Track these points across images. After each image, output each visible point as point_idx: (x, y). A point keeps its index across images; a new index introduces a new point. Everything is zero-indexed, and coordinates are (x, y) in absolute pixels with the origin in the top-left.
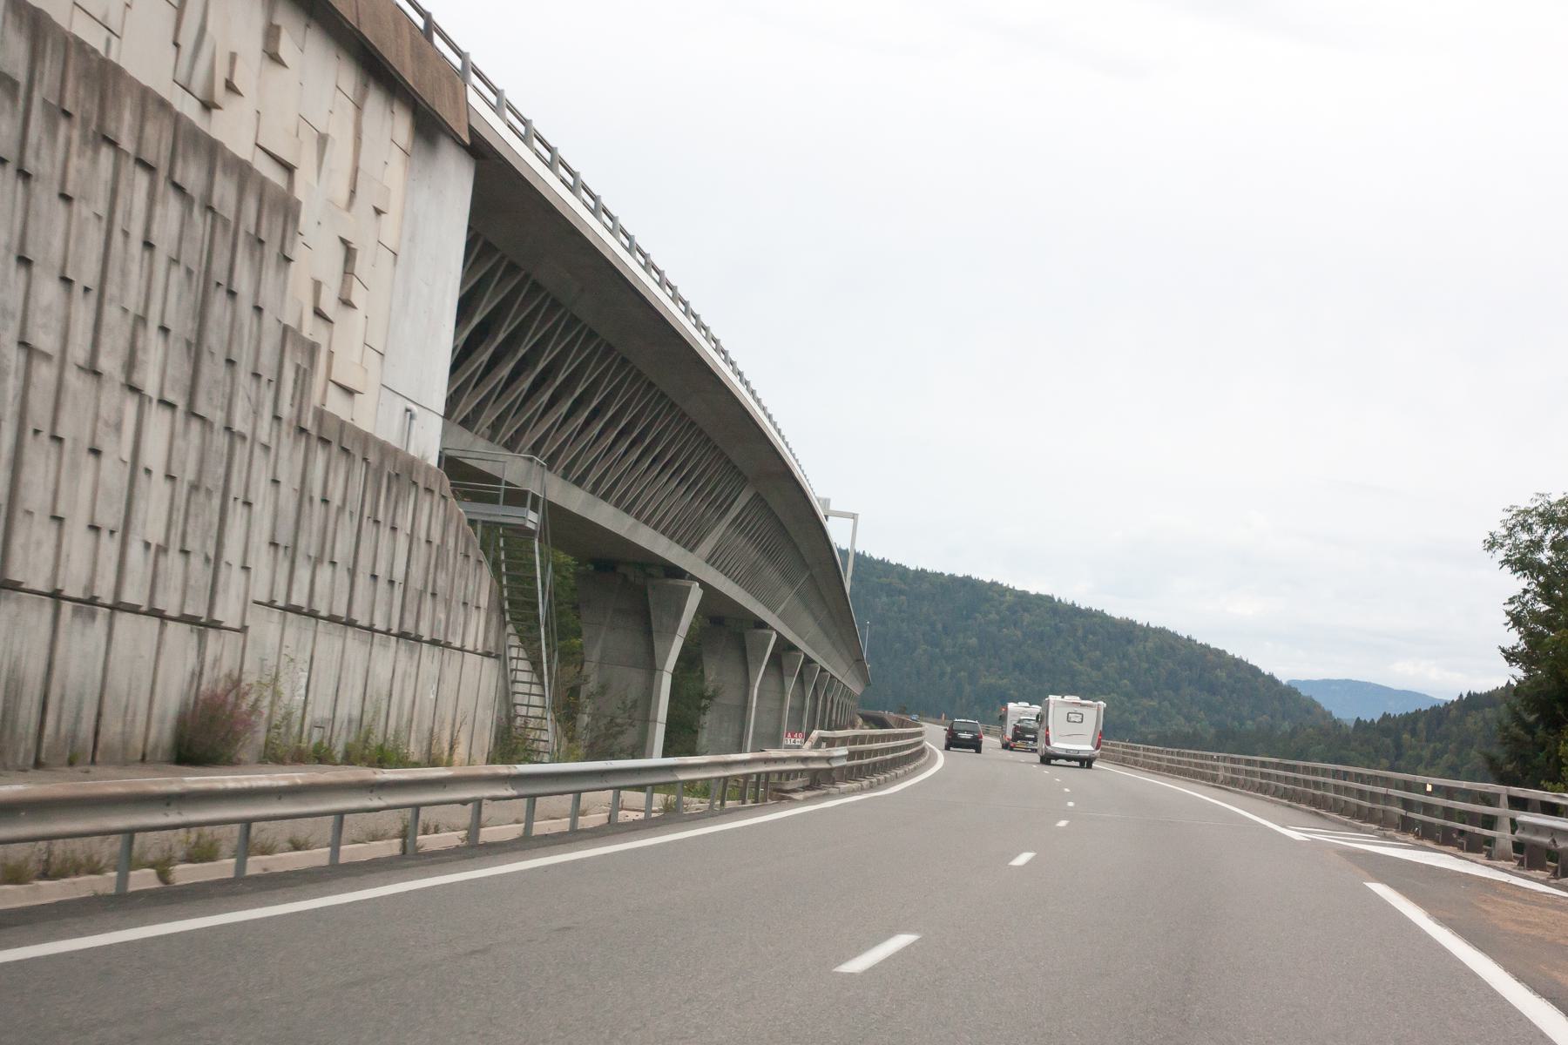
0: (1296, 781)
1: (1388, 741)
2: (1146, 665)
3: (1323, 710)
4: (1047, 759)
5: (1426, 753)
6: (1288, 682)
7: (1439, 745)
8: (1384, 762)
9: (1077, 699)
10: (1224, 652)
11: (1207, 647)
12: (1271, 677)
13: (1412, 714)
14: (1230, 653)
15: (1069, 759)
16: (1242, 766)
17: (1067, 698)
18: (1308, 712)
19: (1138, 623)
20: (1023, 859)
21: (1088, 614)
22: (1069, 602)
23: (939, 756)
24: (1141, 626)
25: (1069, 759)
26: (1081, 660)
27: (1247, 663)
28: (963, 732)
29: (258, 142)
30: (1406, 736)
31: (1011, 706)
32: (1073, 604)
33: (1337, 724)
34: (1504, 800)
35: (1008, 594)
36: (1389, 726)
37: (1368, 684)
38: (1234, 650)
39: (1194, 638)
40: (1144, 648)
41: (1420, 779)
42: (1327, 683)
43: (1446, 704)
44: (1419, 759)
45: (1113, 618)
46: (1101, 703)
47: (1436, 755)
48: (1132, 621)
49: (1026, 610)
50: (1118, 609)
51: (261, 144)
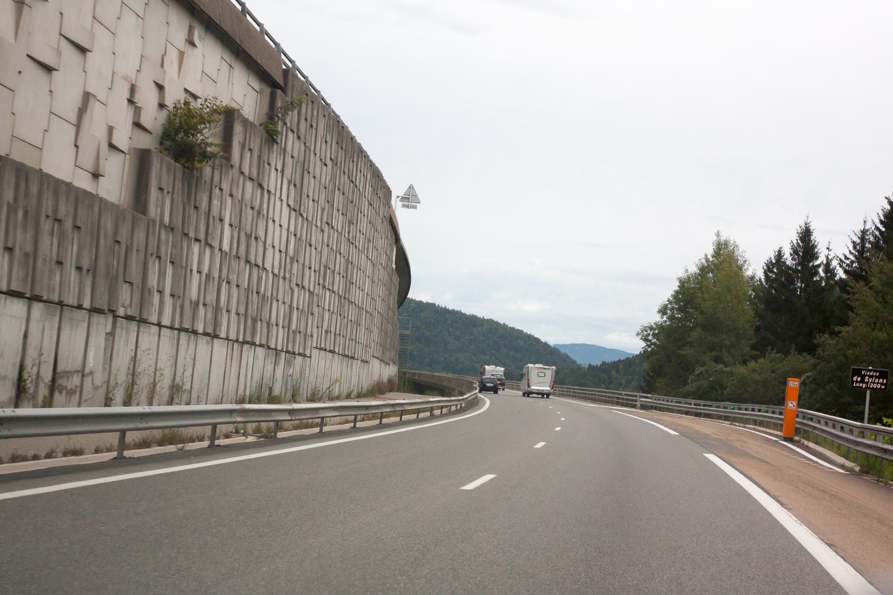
0: (585, 394)
1: (605, 375)
2: (482, 338)
3: (572, 359)
4: (528, 394)
5: (623, 381)
6: (555, 345)
7: (630, 377)
8: (603, 386)
9: (541, 366)
10: (522, 331)
11: (513, 328)
12: (546, 344)
13: (617, 361)
14: (525, 331)
15: (538, 394)
16: (571, 390)
17: (536, 365)
18: (565, 361)
19: (479, 316)
20: (540, 445)
21: (454, 313)
22: (444, 306)
23: (487, 403)
24: (480, 318)
25: (538, 394)
26: (450, 336)
27: (533, 336)
28: (488, 383)
29: (62, 33)
30: (614, 373)
31: (487, 367)
32: (446, 308)
33: (579, 367)
34: (638, 396)
35: (412, 303)
36: (606, 368)
37: (593, 346)
38: (527, 330)
39: (507, 324)
40: (482, 330)
41: (620, 392)
42: (573, 346)
43: (633, 356)
44: (620, 385)
45: (466, 314)
46: (554, 367)
47: (628, 382)
48: (475, 316)
49: (422, 311)
50: (468, 309)
51: (64, 34)
